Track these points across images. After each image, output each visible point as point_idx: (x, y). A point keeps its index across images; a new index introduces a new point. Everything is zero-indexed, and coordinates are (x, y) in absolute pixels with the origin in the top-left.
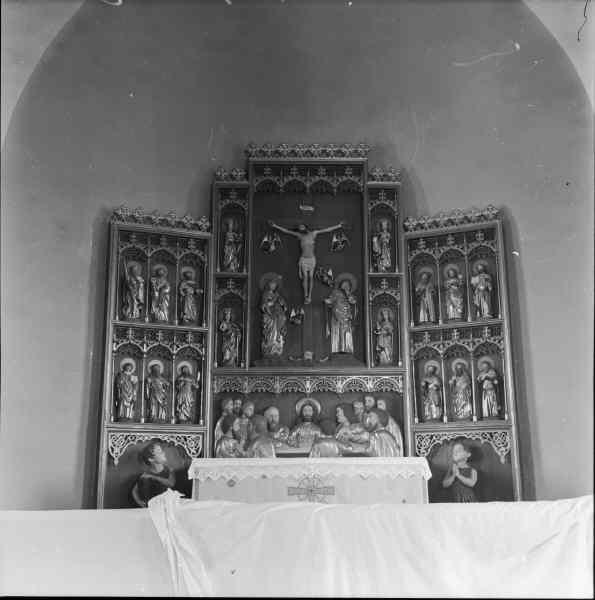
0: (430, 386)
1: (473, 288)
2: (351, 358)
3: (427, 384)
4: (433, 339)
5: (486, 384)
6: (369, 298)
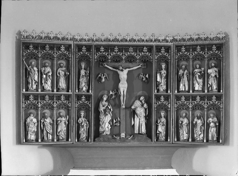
0: (184, 123)
1: (209, 75)
2: (145, 136)
3: (182, 122)
4: (186, 99)
5: (212, 124)
6: (154, 106)
